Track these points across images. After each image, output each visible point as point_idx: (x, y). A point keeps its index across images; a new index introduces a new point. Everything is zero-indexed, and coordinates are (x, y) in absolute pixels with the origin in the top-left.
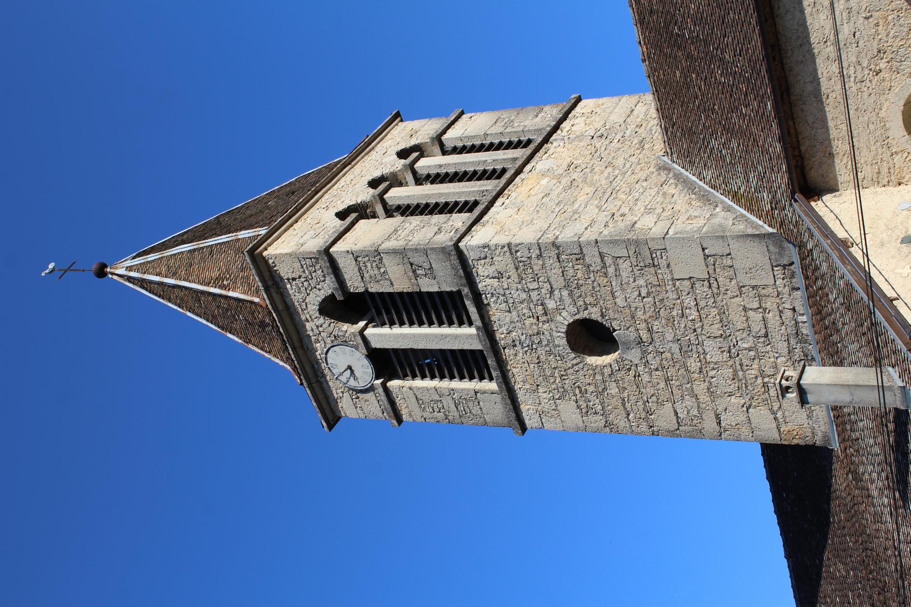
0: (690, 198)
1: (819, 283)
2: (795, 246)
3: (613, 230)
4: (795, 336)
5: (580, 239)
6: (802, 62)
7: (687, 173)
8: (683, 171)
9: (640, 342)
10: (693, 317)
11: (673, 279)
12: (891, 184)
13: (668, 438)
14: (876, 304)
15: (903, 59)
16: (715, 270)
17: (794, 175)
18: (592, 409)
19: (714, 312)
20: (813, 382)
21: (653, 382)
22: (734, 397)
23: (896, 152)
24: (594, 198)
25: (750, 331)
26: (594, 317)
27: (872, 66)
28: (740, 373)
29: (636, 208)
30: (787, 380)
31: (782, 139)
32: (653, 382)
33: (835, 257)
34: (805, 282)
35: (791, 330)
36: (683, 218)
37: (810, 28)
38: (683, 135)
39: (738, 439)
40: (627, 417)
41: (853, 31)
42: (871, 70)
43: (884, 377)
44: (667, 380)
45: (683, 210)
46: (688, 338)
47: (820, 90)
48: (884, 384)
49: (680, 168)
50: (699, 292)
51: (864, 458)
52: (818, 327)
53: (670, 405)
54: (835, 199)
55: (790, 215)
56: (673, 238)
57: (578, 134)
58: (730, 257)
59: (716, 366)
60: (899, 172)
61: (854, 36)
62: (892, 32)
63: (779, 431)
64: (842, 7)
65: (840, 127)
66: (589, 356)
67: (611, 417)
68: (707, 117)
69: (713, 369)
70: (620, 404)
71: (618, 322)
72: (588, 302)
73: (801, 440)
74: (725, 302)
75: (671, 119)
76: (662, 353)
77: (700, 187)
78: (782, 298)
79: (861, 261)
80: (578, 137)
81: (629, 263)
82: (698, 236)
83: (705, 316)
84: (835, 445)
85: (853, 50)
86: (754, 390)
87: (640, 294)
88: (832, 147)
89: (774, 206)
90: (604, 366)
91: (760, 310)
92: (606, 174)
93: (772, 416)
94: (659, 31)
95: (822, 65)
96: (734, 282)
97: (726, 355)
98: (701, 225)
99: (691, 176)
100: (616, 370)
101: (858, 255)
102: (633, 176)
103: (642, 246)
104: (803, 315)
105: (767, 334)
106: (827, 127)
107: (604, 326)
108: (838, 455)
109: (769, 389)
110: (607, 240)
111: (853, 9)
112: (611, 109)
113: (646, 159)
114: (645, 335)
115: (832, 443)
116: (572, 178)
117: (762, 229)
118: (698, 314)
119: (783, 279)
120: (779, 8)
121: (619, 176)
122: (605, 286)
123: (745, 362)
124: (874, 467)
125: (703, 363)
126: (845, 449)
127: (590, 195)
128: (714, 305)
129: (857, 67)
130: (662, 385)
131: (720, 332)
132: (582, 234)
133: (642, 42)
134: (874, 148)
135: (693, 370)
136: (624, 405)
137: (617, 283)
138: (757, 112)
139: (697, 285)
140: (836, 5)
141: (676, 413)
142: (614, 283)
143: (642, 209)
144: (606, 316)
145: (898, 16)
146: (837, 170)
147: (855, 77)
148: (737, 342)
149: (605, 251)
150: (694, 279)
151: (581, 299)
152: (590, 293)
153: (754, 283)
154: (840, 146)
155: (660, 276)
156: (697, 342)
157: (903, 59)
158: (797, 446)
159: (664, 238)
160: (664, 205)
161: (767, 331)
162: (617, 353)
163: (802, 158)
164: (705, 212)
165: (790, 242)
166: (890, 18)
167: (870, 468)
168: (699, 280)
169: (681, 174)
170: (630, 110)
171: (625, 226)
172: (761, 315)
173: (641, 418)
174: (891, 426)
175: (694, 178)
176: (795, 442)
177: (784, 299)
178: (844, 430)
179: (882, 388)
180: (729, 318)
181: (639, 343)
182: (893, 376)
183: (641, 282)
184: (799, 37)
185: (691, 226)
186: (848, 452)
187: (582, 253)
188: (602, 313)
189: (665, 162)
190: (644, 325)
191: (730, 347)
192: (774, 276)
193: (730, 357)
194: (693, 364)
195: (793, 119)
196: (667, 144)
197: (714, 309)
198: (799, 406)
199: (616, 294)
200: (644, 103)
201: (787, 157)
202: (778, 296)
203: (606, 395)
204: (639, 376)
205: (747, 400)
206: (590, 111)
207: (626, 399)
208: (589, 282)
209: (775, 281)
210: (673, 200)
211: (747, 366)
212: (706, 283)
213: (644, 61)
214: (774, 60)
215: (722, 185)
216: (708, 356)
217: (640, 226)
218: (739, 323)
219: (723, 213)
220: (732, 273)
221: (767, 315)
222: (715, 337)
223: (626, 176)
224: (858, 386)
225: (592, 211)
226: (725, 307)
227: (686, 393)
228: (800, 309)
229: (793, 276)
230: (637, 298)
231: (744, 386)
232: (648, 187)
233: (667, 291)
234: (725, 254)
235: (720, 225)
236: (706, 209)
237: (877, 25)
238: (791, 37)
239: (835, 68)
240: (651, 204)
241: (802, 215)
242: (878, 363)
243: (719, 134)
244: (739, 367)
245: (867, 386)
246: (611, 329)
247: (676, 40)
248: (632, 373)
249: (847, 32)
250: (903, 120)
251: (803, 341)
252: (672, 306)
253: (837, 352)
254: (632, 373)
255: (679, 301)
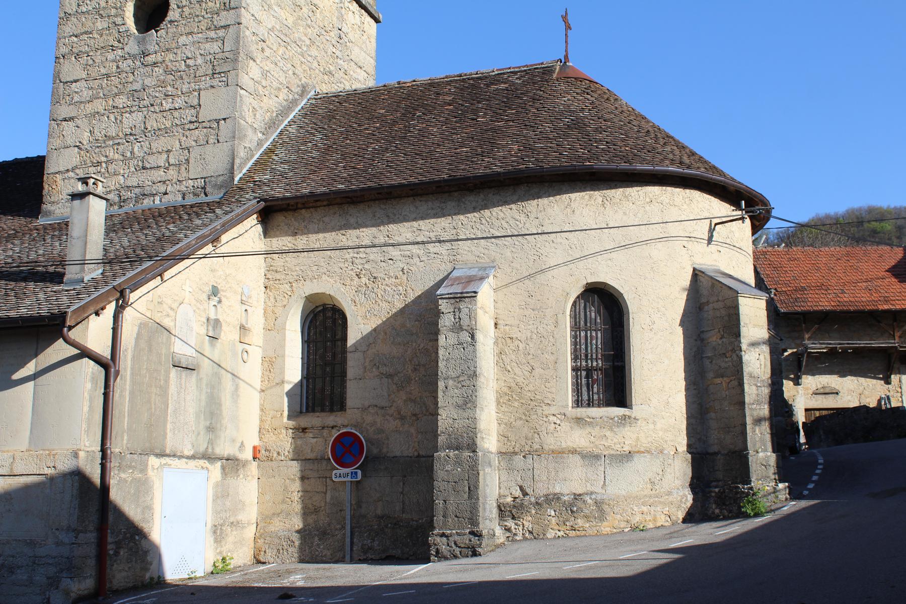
0: (273, 111)
1: (186, 217)
2: (220, 199)
3: (249, 39)
4: (142, 193)
5: (243, 9)
6: (374, 216)
7: (297, 110)
8: (299, 107)
9: (145, 54)
10: (164, 105)
11: (200, 90)
12: (267, 280)
13: (53, 72)
14: (159, 262)
15: (366, 296)
16: (205, 128)
17: (280, 203)
18: (83, 2)
19: (168, 124)
20: (90, 206)
21: (107, 62)
22: (89, 134)
23: (292, 286)
24: (282, 25)
25: (149, 154)
26: (170, 13)
27: (364, 272)
28: (111, 143)
29: (268, 63)
30: (94, 184)
31: (312, 194)
32: (107, 62)
33: (205, 231)
34: (189, 205)
35: (147, 190)
36: (255, 103)
37: (401, 225)
38: (330, 111)
39: (50, 136)
40: (73, 35)
41: (394, 259)
42: (361, 270)
43: (94, 265)
44: (108, 76)
45: (262, 104)
46: (146, 98)
47: (350, 229)
48: (86, 265)
49: (302, 105)
50: (187, 112)
51: (27, 245)
52: (148, 213)
53: (84, 76)
54: (257, 235)
55: (247, 196)
56: (237, 94)
57: (345, 17)
58: (216, 142)
59: (118, 121)
60: (275, 288)
61: (390, 259)
62: (389, 289)
63: (57, 173)
64: (414, 251)
65: (318, 243)
66: (134, 5)
67: (74, 19)
68: (341, 133)
69: (116, 119)
70: (86, 29)
71: (164, 36)
72: (184, 10)
73: (47, 191)
74: (176, 134)
75: (345, 102)
76: (133, 73)
77: (283, 121)
78: (176, 184)
79: (199, 253)
80: (342, 16)
81: (217, 52)
82: (237, 116)
83: (165, 115)
84: (42, 221)
85: (379, 258)
86: (95, 153)
87: (189, 58)
88: (302, 235)
89: (257, 183)
90: (123, 18)
91: (167, 165)
92: (304, 38)
93: (70, 168)
94: (420, 99)
95: (369, 232)
96: (194, 143)
97: (128, 131)
98: (247, 119)
99: (294, 114)
100: (119, 29)
101: (205, 251)
102: (299, 63)
103: (232, 64)
104: (161, 201)
105: (145, 169)
106: (318, 233)
107: (161, 22)
108: (32, 223)
109: (95, 166)
110: (240, 34)
111: (411, 260)
112: (365, 49)
113: (314, 76)
114: (150, 59)
115: (44, 219)
116: (303, 8)
117: (238, 171)
118: (167, 109)
119: (193, 186)
120: (421, 201)
121: (301, 50)
122: (198, 27)
123: (121, 148)
124: (18, 253)
125: (122, 110)
126: (37, 230)
127: (285, 22)
128: (174, 124)
129: (365, 260)
130: (103, 71)
131: (149, 128)
132: (247, 10)
133: (414, 83)
134: (297, 269)
135: (116, 100)
136: (86, 33)
137: (201, 38)
138: (338, 176)
139: (193, 111)
140: (416, 246)
141: (76, 81)
142: (200, 35)
143: (267, 68)
144: (171, 25)
145: (401, 294)
146: (282, 238)
147: (357, 258)
148: (140, 142)
149: (230, 30)
150: (198, 109)
151: (188, 3)
152: (192, 12)
153: (192, 161)
154: (302, 241)
155: (203, 78)
156: (141, 106)
157: (366, 296)
158: (42, 188)
159: (237, 85)
160: (268, 88)
161: (147, 169)
162: (136, 31)
163: (295, 210)
164: (259, 124)
165: (224, 195)
166: (400, 288)
167: (17, 249)
168: (198, 113)
169: (297, 105)
170: (362, 65)
171: (251, 52)
172: (163, 165)
173: (72, 48)
174: (51, 269)
175: (291, 117)
176: (46, 186)
177: (175, 185)
178: (54, 229)
179: (83, 263)
180: (161, 137)
181: (143, 53)
182: (96, 272)
183: (200, 61)
184: (395, 215)
185: (246, 110)
186: (35, 231)
187: (230, 9)
188: (173, 22)
189: (310, 92)
190: (160, 59)
191: (135, 135)
192: (196, 179)
193: (126, 135)
194: (121, 101)
195: (328, 205)
196: (325, 95)
197: (170, 124)
198: (70, 192)
199: (190, 36)
200: (367, 79)
201: (296, 197)
202: (179, 181)
203: (95, 17)
204: (113, 50)
205: (86, 147)
206: (365, 29)
207: (91, 36)
208: (204, 13)
209: (191, 179)
210: (273, 96)
211: (117, 149)
212: (194, 119)
213: (399, 83)
214: (378, 194)
215: (282, 140)
216: (128, 115)
217: (251, 65)
218: (156, 145)
219: (257, 139)
220: (202, 142)
221: (162, 170)
222: (145, 123)
223: (300, 57)
224: (86, 243)
225: (269, 22)
226: (172, 134)
227: (94, 92)
228: (166, 199)
229: (196, 195)
230: (185, 56)
231: (99, 145)
232: (287, 75)
233: (189, 83)
234: (219, 137)
235: (245, 136)
236: (262, 125)
237: (396, 278)
238: (395, 208)
239: (367, 242)
240: (271, 76)
241: (245, 207)
242: (107, 261)
243: (325, 142)
244: (116, 141)
245: (86, 251)
246: (158, 29)
247: (410, 113)
248: (116, 44)
249: (393, 254)
250: (318, 293)
251: (137, 199)
252: (176, 86)
253: (123, 228)
254: (116, 44)
255: (180, 93)
